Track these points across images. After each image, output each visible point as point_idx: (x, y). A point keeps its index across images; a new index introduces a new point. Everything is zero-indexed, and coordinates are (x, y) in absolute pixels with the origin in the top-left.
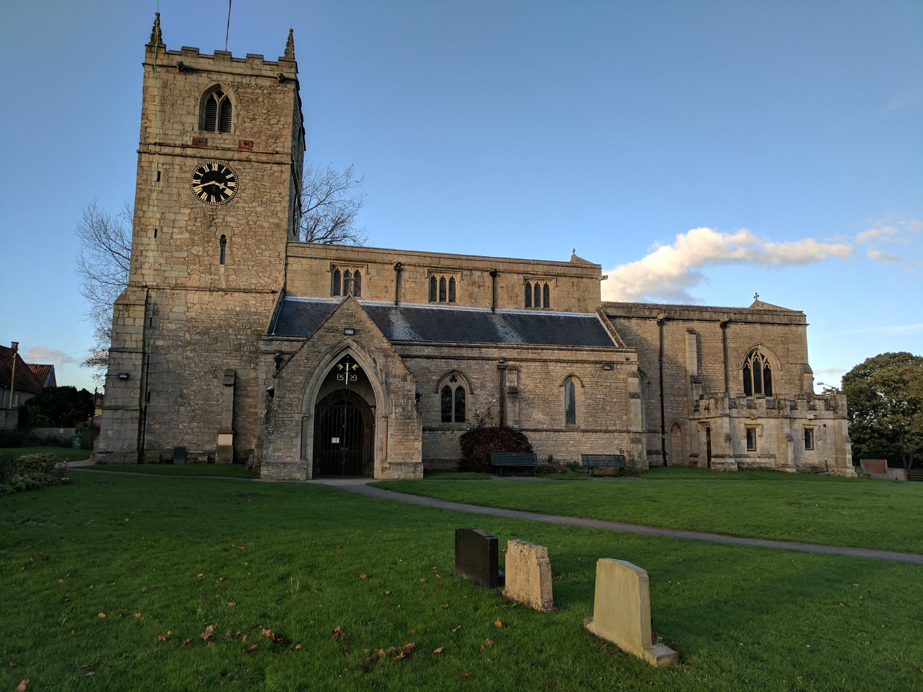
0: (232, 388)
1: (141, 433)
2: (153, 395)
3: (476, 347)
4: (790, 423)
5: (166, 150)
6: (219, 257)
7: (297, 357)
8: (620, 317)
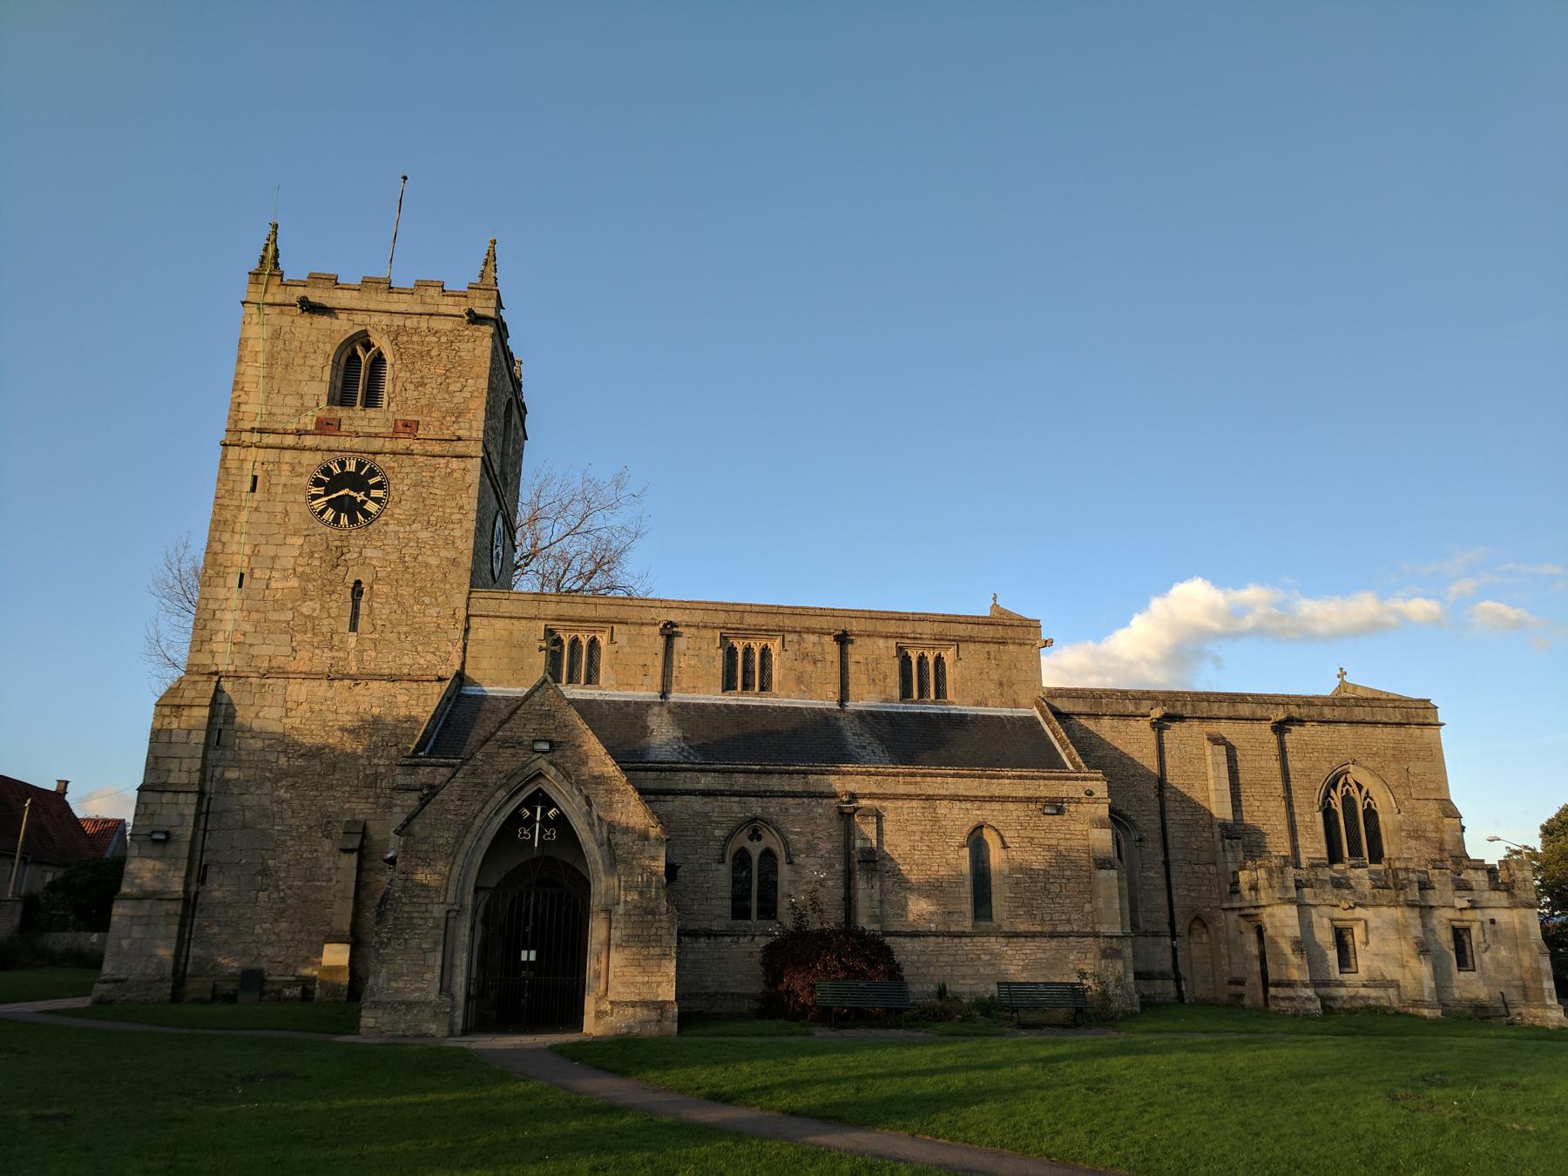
0: (355, 855)
1: (182, 943)
2: (212, 870)
3: (798, 772)
4: (1422, 917)
6: (348, 619)
7: (443, 795)
8: (1079, 715)
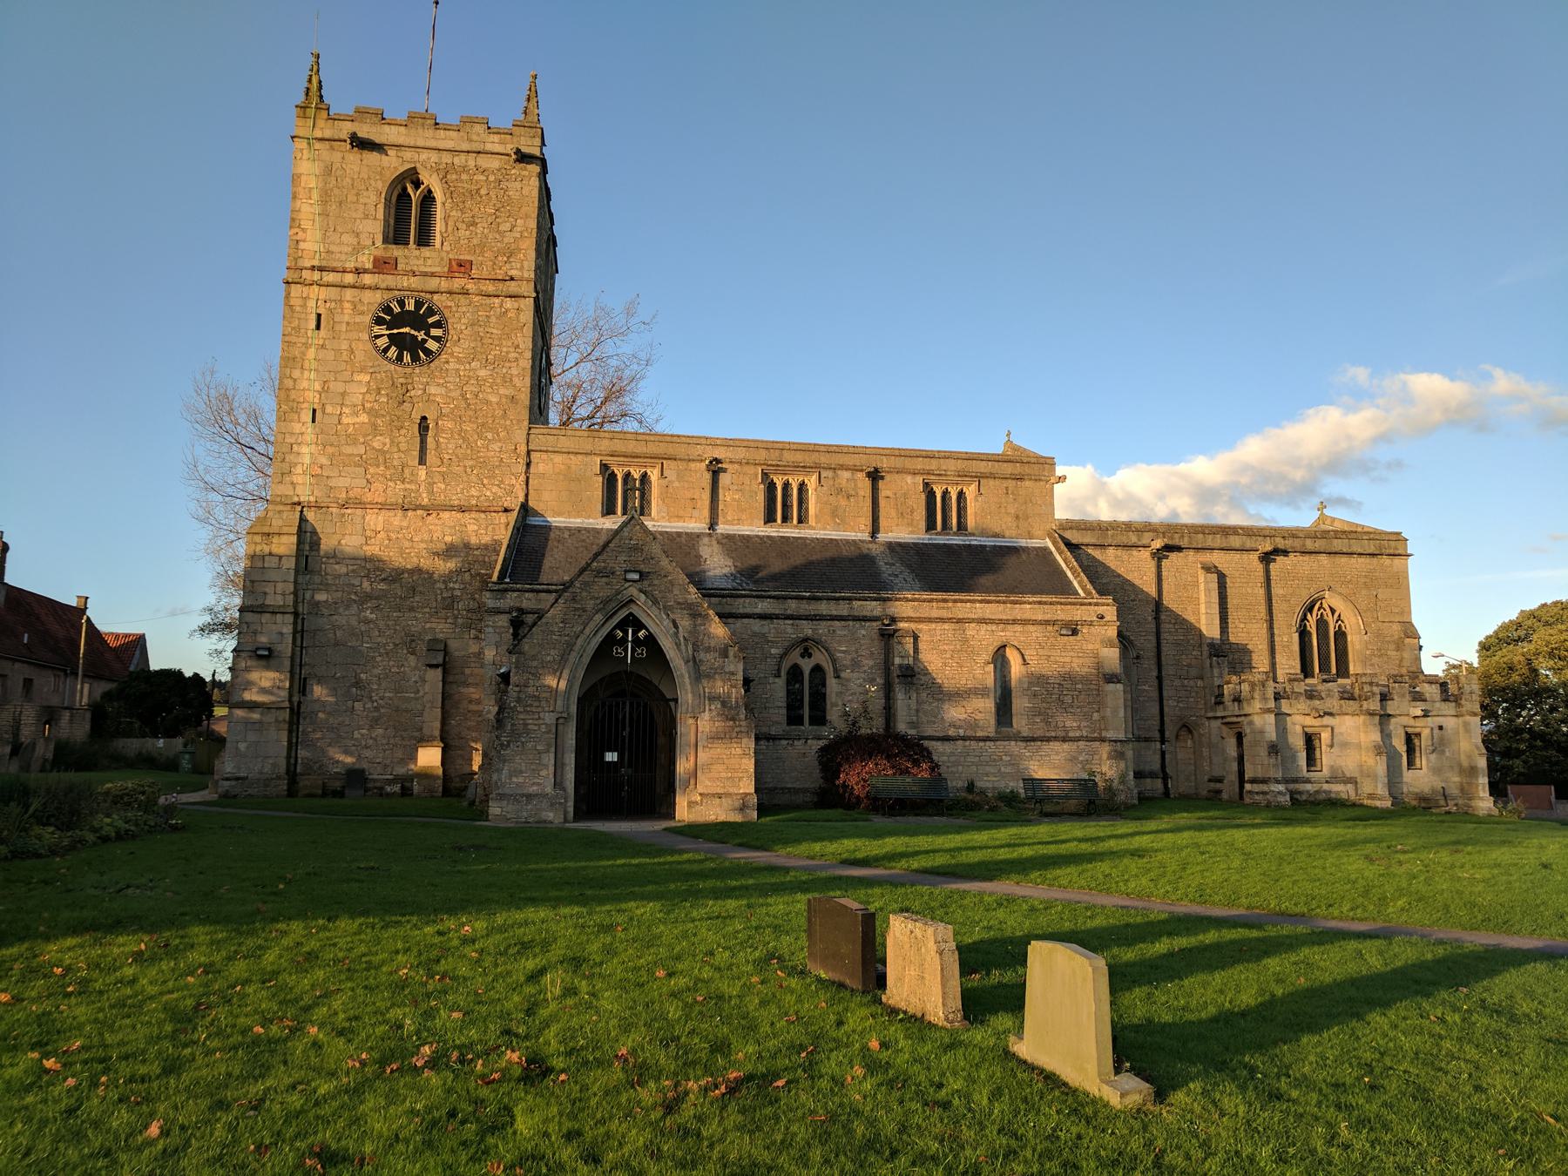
0: (440, 670)
1: (292, 746)
3: (844, 599)
5: (330, 277)
6: (416, 453)
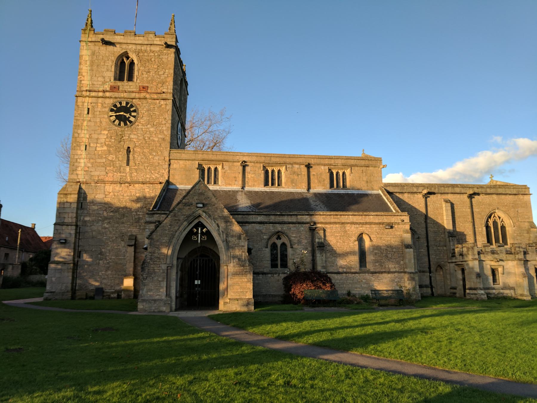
0: (133, 247)
1: (74, 278)
3: (294, 215)
5: (93, 94)
6: (125, 161)
